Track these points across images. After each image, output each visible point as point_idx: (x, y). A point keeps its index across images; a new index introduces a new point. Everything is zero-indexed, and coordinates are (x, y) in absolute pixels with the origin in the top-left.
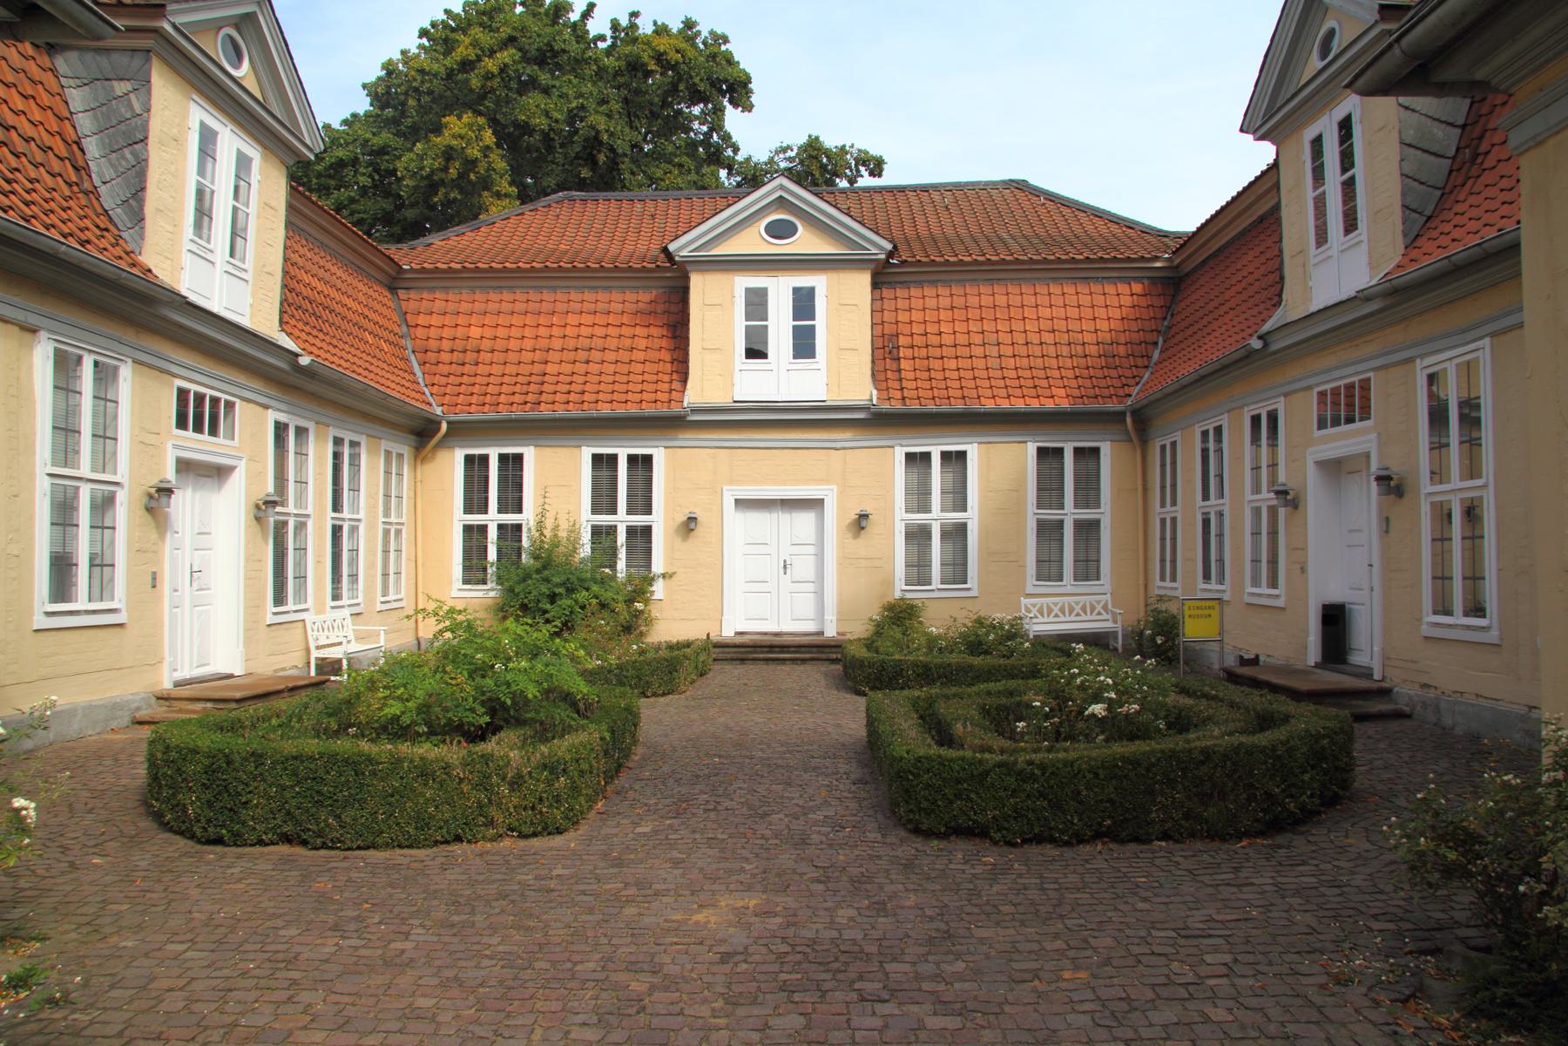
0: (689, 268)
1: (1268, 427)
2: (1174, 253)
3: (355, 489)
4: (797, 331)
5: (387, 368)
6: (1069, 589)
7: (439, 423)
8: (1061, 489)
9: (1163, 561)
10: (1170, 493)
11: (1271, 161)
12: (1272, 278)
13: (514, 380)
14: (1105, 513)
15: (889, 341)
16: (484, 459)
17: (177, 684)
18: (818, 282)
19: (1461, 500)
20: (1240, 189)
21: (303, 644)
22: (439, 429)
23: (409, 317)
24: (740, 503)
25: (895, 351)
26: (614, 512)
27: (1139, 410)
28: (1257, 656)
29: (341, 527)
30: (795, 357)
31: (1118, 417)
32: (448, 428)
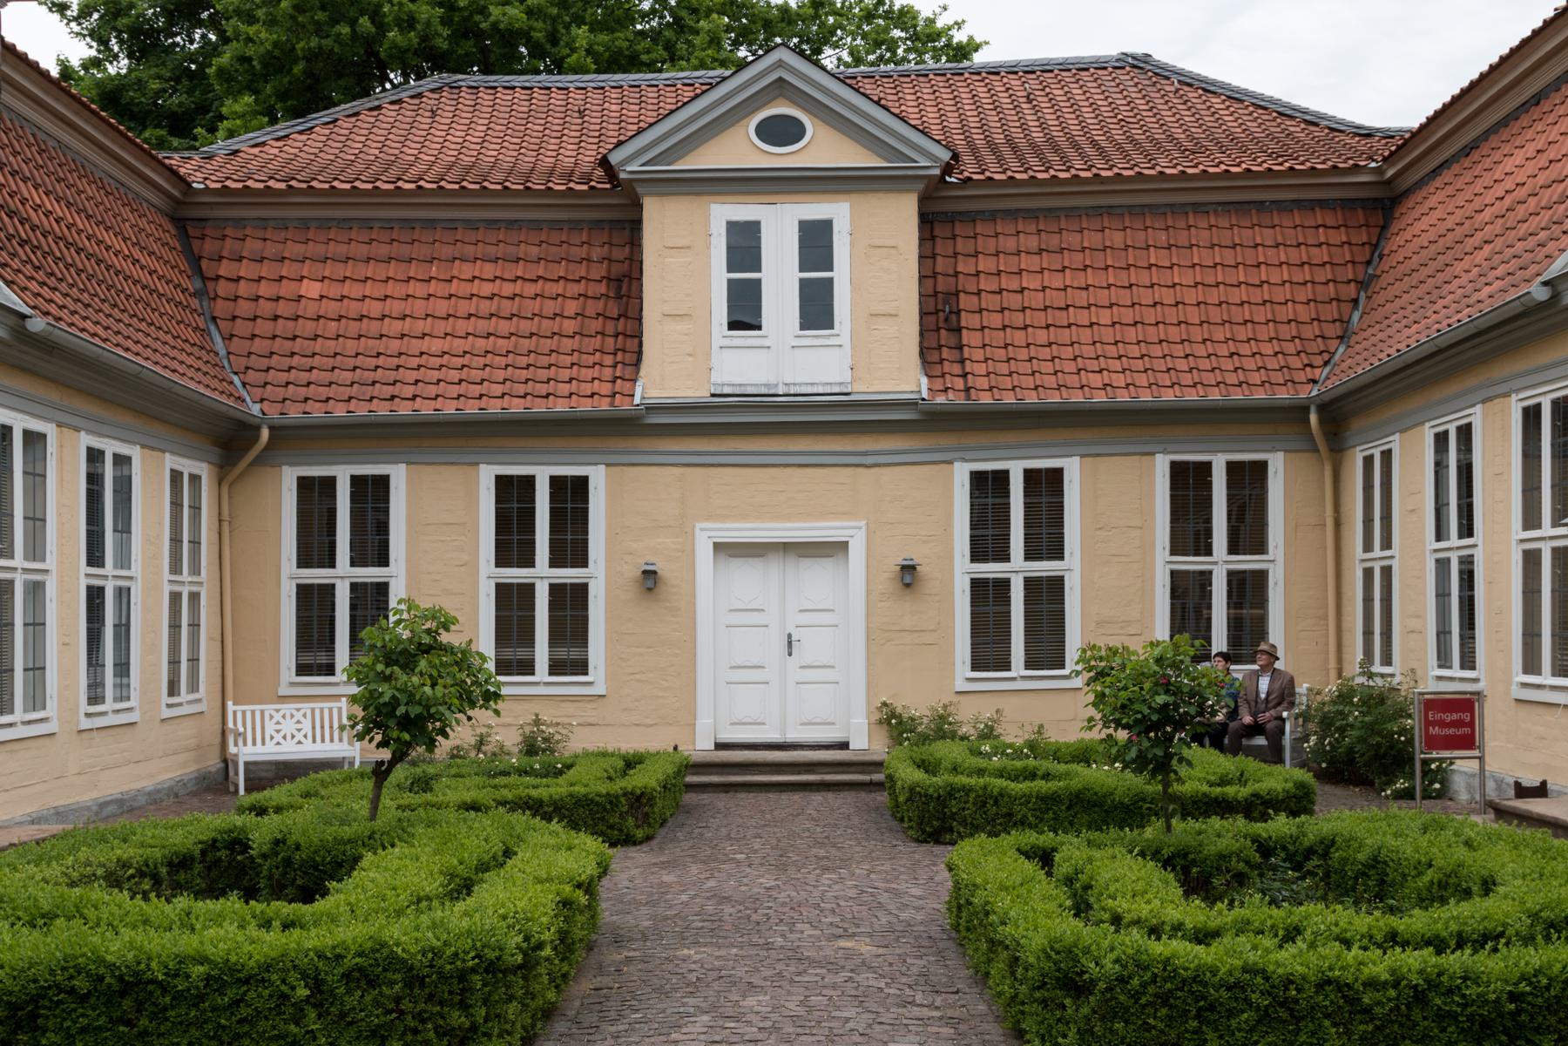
0: (640, 190)
2: (1385, 159)
3: (124, 528)
5: (172, 342)
7: (257, 428)
10: (1381, 529)
14: (1276, 561)
15: (946, 302)
16: (329, 484)
18: (837, 211)
21: (218, 727)
22: (257, 438)
23: (204, 264)
24: (719, 547)
25: (954, 317)
28: (1544, 783)
29: (101, 590)
30: (802, 328)
31: (1298, 412)
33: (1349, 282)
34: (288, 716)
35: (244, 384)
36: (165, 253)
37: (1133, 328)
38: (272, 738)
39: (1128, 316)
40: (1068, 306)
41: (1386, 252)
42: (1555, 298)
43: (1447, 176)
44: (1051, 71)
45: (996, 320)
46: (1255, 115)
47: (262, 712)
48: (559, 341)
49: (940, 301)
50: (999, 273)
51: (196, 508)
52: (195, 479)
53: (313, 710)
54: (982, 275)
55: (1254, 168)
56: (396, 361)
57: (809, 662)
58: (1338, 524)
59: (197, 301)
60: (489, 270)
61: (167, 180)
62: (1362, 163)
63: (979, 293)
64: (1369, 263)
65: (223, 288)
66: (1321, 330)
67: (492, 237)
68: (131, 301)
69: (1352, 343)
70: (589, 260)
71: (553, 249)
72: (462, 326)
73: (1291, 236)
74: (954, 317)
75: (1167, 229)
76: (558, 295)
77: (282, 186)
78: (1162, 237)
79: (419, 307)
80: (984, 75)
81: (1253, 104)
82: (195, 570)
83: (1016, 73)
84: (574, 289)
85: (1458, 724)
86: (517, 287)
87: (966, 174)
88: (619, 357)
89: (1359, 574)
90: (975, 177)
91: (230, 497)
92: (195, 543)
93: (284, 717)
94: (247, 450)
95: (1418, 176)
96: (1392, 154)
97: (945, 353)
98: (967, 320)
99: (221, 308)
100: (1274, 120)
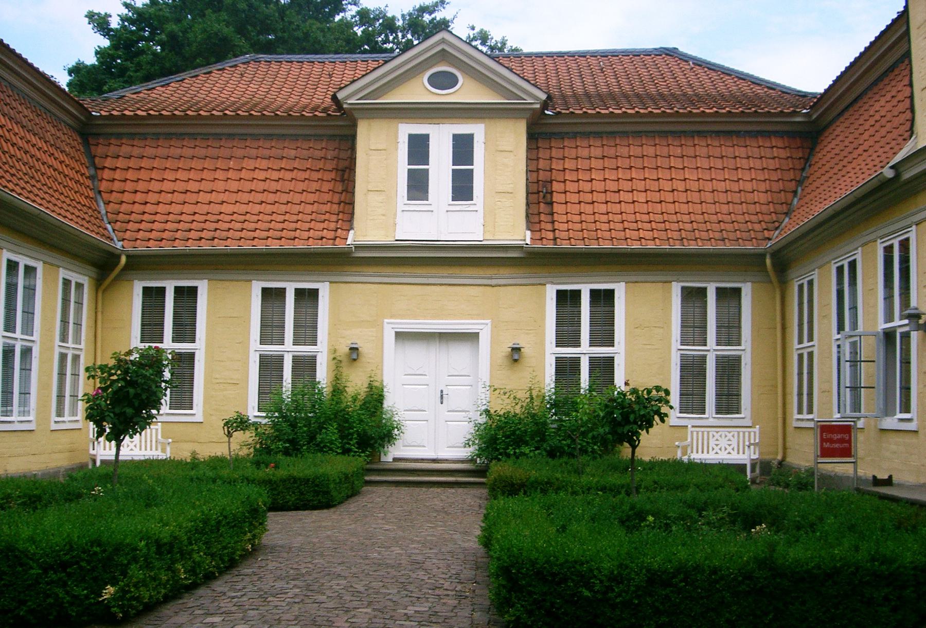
0: (356, 115)
1: (901, 288)
2: (811, 107)
4: (425, 159)
6: (711, 422)
7: (119, 257)
8: (704, 327)
9: (800, 394)
11: (902, 9)
12: (902, 108)
13: (191, 218)
14: (745, 350)
15: (544, 186)
18: (477, 130)
19: (22, 346)
20: (873, 39)
23: (97, 160)
24: (400, 336)
25: (549, 196)
26: (577, 344)
27: (780, 250)
28: (890, 477)
33: (791, 180)
34: (723, 436)
35: (114, 230)
36: (72, 152)
37: (659, 205)
38: (713, 449)
39: (656, 197)
40: (620, 190)
41: (813, 163)
42: (897, 176)
43: (846, 115)
44: (617, 56)
45: (574, 198)
46: (738, 83)
48: (305, 207)
49: (540, 186)
50: (577, 170)
51: (79, 303)
52: (79, 286)
54: (567, 171)
55: (733, 111)
57: (454, 408)
58: (784, 328)
59: (90, 182)
60: (264, 164)
61: (76, 110)
62: (798, 110)
63: (565, 181)
64: (803, 169)
65: (107, 174)
66: (775, 209)
67: (268, 144)
68: (45, 177)
69: (792, 216)
70: (326, 159)
71: (305, 152)
72: (245, 197)
73: (756, 152)
74: (549, 196)
75: (681, 146)
76: (306, 179)
77: (144, 114)
78: (678, 151)
79: (220, 186)
80: (576, 57)
81: (737, 77)
82: (77, 340)
83: (596, 56)
84: (316, 176)
85: (841, 441)
86: (282, 174)
87: (558, 110)
88: (341, 216)
89: (796, 358)
90: (563, 111)
92: (78, 325)
93: (721, 436)
94: (112, 270)
95: (830, 118)
96: (815, 104)
97: (543, 217)
98: (556, 197)
99: (104, 186)
100: (749, 86)
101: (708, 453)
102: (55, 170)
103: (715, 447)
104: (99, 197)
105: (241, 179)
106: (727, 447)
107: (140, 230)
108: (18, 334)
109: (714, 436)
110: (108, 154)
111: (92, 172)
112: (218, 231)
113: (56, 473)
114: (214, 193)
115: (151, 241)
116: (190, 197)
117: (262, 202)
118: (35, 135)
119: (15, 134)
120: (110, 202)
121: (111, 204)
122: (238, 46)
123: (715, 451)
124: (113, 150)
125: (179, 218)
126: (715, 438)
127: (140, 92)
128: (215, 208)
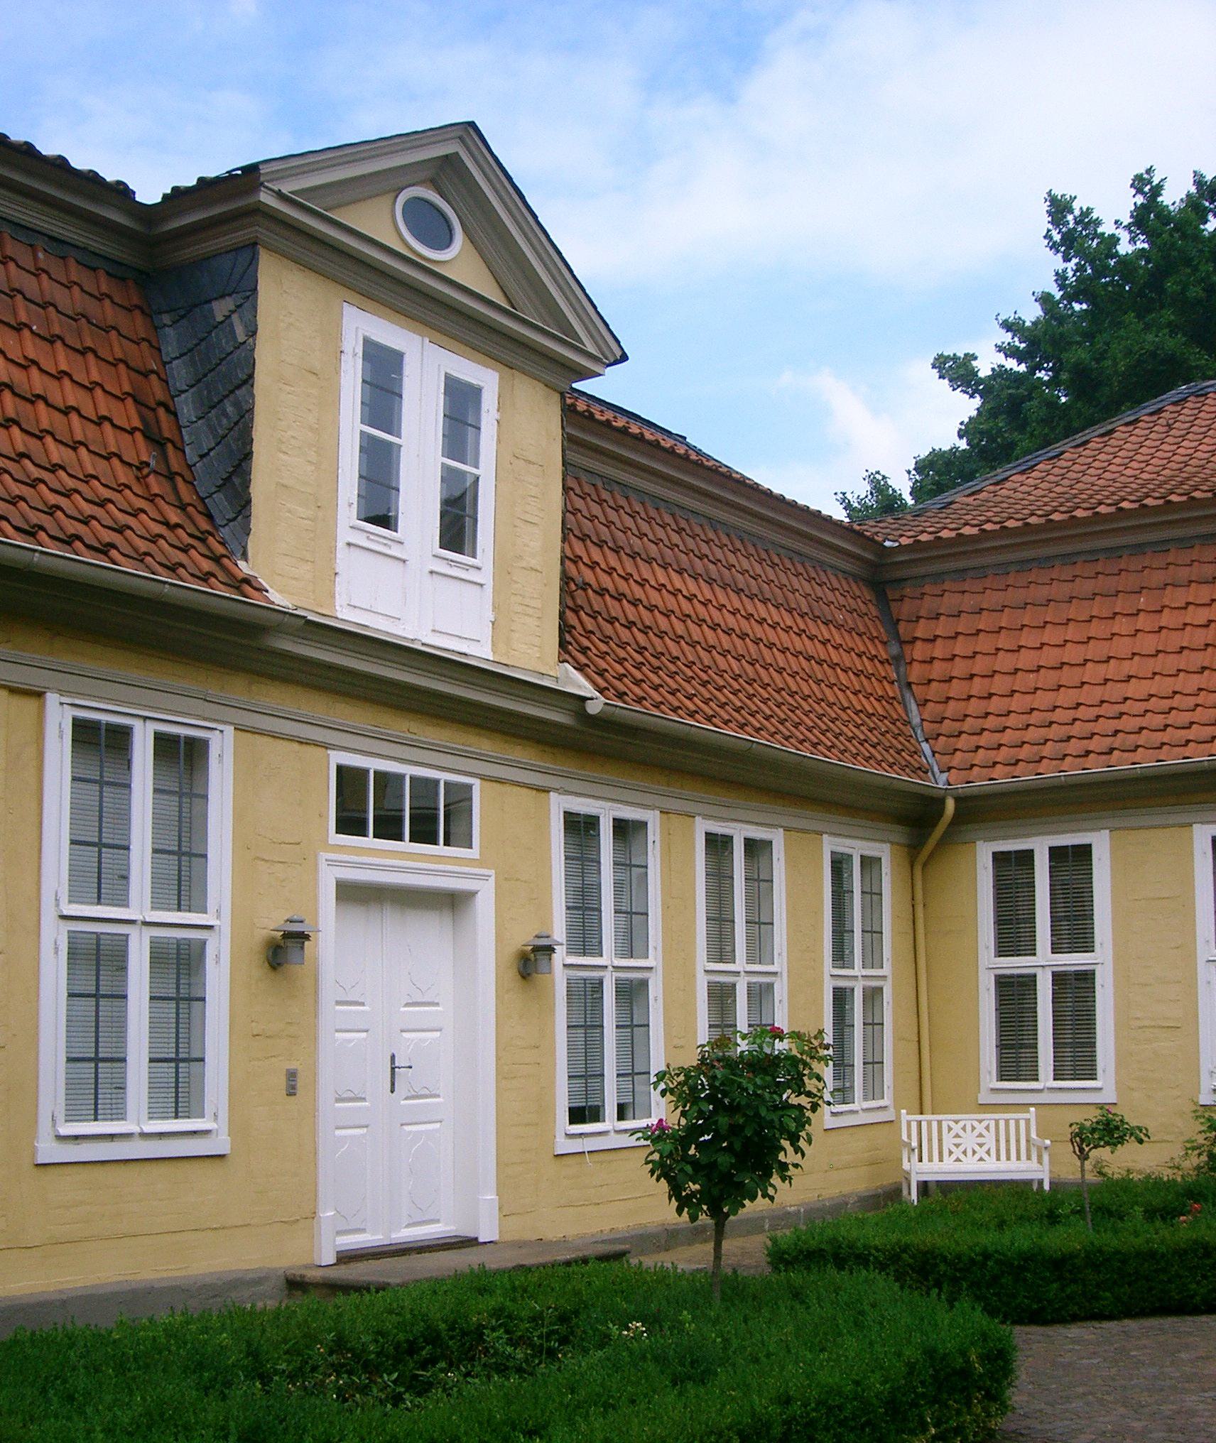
7: (942, 801)
17: (346, 1258)
32: (956, 809)
34: (969, 1128)
35: (934, 753)
38: (951, 1153)
47: (940, 1123)
52: (869, 863)
53: (997, 1121)
56: (1144, 706)
61: (854, 544)
65: (919, 651)
72: (1170, 663)
75: (101, 783)
77: (975, 531)
79: (1122, 647)
91: (924, 880)
92: (873, 932)
93: (964, 1129)
94: (935, 825)
99: (916, 673)
101: (941, 1160)
102: (809, 658)
103: (953, 1149)
104: (908, 695)
105: (1161, 628)
106: (977, 1148)
107: (978, 747)
108: (740, 964)
109: (950, 1129)
110: (920, 614)
111: (894, 649)
112: (1120, 735)
113: (838, 1207)
114: (1112, 661)
115: (998, 766)
116: (1068, 676)
117: (1204, 668)
118: (765, 601)
119: (721, 607)
120: (927, 701)
121: (930, 705)
122: (1197, 367)
123: (954, 1157)
124: (928, 605)
125: (1049, 716)
126: (953, 1133)
127: (981, 491)
128: (1115, 691)
